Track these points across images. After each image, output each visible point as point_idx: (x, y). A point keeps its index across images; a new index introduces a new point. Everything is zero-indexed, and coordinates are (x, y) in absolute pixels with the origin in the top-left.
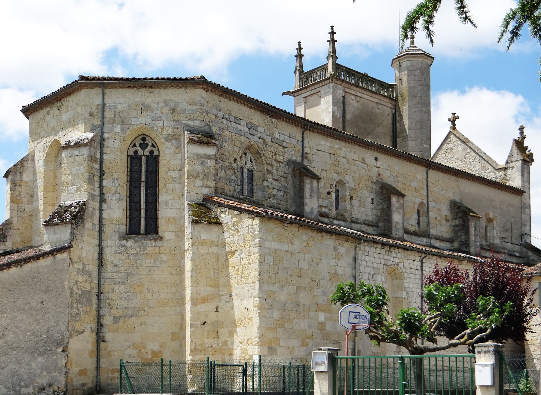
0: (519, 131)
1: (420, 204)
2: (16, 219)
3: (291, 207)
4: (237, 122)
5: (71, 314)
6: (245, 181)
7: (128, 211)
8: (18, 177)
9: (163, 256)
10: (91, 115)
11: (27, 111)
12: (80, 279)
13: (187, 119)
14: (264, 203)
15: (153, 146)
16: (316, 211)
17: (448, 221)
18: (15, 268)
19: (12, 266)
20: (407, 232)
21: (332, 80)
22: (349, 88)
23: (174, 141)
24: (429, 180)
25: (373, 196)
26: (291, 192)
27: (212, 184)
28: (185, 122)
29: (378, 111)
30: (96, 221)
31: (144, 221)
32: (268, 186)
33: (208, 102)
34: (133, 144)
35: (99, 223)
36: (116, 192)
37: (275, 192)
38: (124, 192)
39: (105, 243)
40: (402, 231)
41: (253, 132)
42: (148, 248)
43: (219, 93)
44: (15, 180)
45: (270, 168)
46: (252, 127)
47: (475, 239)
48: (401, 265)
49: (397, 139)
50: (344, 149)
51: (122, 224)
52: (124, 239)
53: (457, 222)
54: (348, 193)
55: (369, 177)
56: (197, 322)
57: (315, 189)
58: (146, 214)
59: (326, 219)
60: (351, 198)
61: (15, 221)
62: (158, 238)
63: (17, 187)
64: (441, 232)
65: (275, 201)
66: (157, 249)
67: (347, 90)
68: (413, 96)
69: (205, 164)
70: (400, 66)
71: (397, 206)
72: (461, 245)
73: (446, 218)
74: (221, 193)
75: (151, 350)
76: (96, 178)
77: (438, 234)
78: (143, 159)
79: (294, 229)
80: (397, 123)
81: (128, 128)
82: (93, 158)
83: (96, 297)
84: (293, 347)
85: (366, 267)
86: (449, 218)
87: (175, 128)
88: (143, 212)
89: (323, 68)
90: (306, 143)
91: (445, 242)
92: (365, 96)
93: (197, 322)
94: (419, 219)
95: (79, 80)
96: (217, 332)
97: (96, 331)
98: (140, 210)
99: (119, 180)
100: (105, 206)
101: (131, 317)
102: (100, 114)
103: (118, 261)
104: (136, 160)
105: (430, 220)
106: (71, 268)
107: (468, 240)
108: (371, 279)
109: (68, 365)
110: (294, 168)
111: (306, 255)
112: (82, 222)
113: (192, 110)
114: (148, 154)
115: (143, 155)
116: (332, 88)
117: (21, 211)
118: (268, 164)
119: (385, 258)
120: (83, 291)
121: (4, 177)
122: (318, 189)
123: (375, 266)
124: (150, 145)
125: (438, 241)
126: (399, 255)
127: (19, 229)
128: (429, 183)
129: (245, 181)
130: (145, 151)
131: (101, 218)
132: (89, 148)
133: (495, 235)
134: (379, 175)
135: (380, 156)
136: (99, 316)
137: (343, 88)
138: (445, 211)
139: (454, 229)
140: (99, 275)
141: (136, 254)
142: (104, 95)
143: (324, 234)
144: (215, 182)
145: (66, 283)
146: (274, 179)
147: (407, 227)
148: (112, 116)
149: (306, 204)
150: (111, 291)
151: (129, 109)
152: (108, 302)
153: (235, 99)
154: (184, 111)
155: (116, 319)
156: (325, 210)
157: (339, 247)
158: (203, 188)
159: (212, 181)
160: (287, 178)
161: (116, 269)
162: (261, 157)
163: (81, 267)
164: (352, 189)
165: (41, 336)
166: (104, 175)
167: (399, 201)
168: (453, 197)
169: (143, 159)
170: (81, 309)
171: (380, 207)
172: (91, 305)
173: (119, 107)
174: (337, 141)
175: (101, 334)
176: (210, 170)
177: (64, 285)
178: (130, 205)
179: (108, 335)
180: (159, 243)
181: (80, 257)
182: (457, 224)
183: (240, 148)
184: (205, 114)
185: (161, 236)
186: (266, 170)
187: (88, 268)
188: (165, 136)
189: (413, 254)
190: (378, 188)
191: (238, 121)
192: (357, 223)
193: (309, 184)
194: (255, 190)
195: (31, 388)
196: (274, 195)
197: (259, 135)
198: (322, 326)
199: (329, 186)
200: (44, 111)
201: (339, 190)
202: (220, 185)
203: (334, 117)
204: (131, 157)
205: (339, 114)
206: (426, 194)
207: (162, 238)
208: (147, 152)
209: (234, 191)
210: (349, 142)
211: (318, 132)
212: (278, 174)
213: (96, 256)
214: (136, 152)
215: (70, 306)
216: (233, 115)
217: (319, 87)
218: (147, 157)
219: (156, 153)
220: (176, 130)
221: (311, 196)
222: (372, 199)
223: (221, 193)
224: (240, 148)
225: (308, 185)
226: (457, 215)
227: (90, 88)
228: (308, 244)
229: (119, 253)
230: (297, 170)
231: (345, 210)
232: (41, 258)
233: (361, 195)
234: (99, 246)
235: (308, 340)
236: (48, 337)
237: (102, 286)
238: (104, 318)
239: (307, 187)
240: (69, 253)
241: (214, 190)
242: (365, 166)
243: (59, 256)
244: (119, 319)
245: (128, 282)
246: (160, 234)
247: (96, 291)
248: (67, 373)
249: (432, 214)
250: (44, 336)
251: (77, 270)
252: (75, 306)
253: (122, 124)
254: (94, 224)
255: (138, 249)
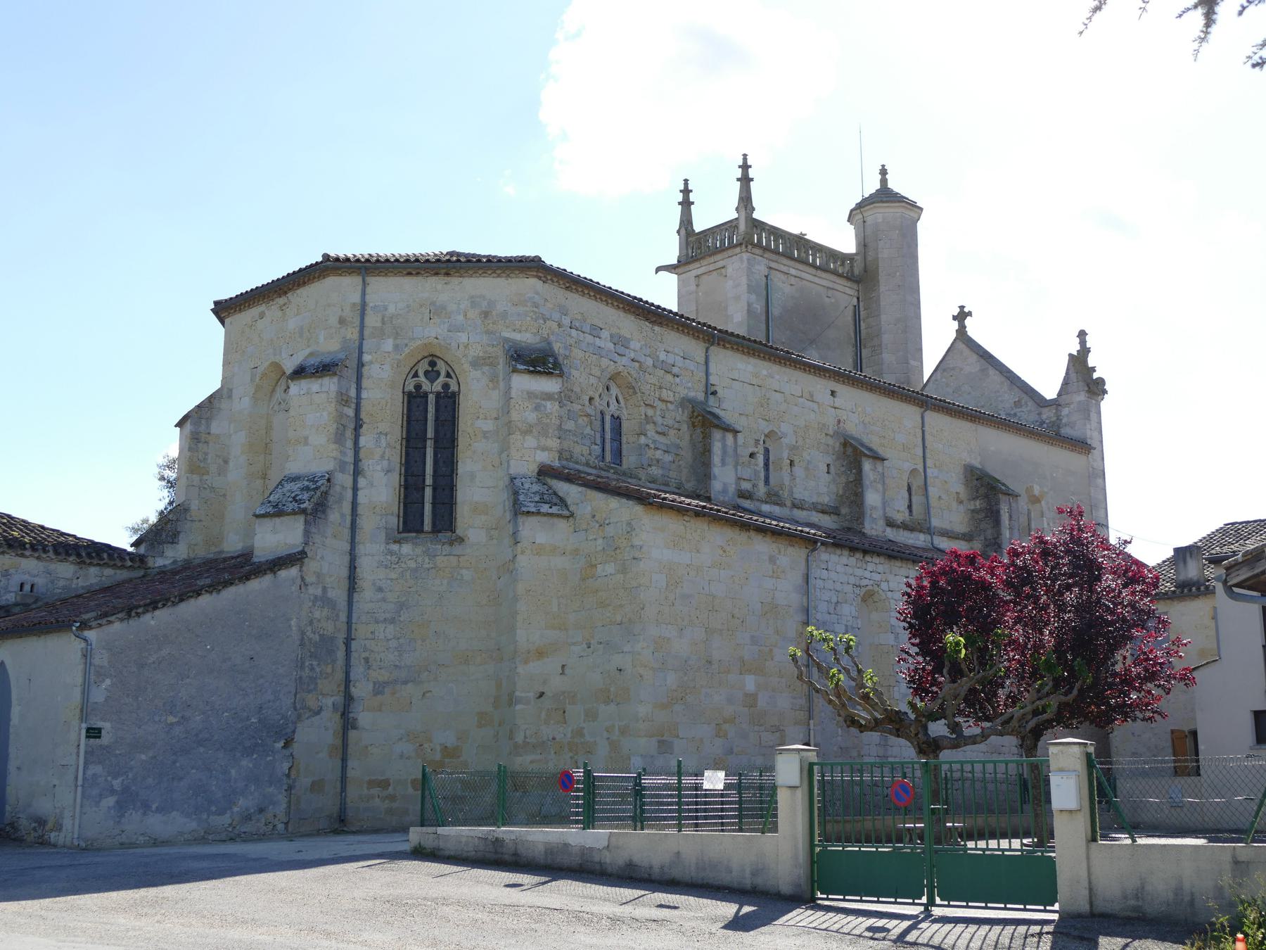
0: (1078, 340)
1: (911, 471)
2: (197, 502)
3: (688, 481)
4: (595, 333)
5: (301, 678)
6: (608, 436)
7: (402, 490)
8: (202, 428)
9: (464, 572)
10: (342, 321)
11: (223, 310)
12: (317, 614)
13: (509, 330)
14: (640, 476)
15: (448, 375)
16: (732, 489)
17: (961, 502)
18: (208, 595)
19: (203, 592)
20: (890, 523)
21: (746, 247)
22: (776, 262)
23: (487, 368)
24: (927, 428)
25: (829, 460)
26: (687, 454)
27: (554, 443)
28: (506, 334)
29: (827, 299)
30: (347, 507)
31: (431, 509)
32: (647, 445)
33: (546, 300)
34: (413, 372)
35: (352, 511)
36: (382, 457)
37: (658, 454)
38: (395, 456)
39: (361, 549)
40: (881, 523)
41: (621, 350)
42: (437, 558)
43: (564, 284)
44: (198, 433)
45: (650, 412)
46: (620, 342)
47: (1011, 534)
48: (884, 586)
49: (863, 350)
50: (777, 377)
51: (392, 514)
52: (395, 542)
53: (978, 504)
54: (785, 455)
55: (820, 425)
56: (528, 694)
57: (730, 451)
58: (434, 497)
59: (749, 501)
60: (792, 463)
61: (194, 505)
62: (456, 540)
63: (200, 445)
64: (951, 522)
65: (660, 472)
66: (453, 559)
67: (773, 265)
68: (889, 275)
69: (543, 408)
70: (864, 222)
71: (872, 478)
72: (987, 546)
73: (958, 497)
74: (567, 459)
75: (441, 744)
76: (349, 434)
77: (944, 526)
78: (431, 398)
79: (700, 526)
80: (862, 322)
81: (406, 345)
82: (345, 399)
83: (343, 648)
84: (701, 740)
85: (823, 591)
86: (963, 496)
87: (488, 345)
88: (428, 492)
89: (730, 227)
90: (712, 369)
91: (957, 541)
92: (804, 275)
93: (528, 694)
94: (910, 500)
95: (322, 262)
96: (564, 712)
97: (341, 709)
98: (424, 489)
99: (389, 437)
100: (362, 482)
101: (405, 683)
102: (357, 321)
103: (384, 581)
104: (419, 399)
105: (930, 502)
106: (302, 595)
107: (998, 537)
108: (832, 612)
109: (293, 772)
110: (693, 412)
111: (722, 571)
112: (324, 512)
113: (519, 315)
114: (439, 389)
115: (431, 392)
116: (746, 261)
117: (204, 488)
118: (646, 405)
119: (856, 574)
120: (321, 636)
121: (176, 426)
122: (735, 450)
123: (838, 586)
124: (443, 373)
125: (945, 539)
126: (880, 568)
127: (200, 521)
128: (926, 433)
129: (608, 436)
130: (435, 384)
131: (354, 505)
132: (339, 380)
133: (1046, 526)
134: (839, 421)
135: (839, 388)
136: (347, 681)
137: (765, 261)
138: (957, 485)
139: (973, 517)
140: (349, 605)
141: (416, 570)
142: (365, 288)
143: (752, 533)
144: (559, 441)
145: (293, 623)
146: (658, 433)
147: (890, 515)
148: (379, 324)
149: (715, 477)
150: (371, 636)
151: (408, 312)
152: (364, 655)
153: (592, 294)
154: (504, 315)
155: (379, 689)
156: (746, 486)
157: (777, 556)
158: (538, 452)
159: (555, 439)
160: (679, 430)
161: (380, 596)
162: (635, 393)
163: (319, 592)
164: (793, 448)
165: (248, 718)
166: (361, 426)
167: (876, 468)
168: (968, 460)
169: (431, 398)
170: (318, 670)
171: (843, 479)
172: (334, 661)
173: (391, 309)
174: (766, 364)
175: (351, 715)
176: (551, 419)
177: (290, 626)
178: (406, 481)
179: (364, 717)
180: (457, 549)
181: (318, 575)
182: (978, 507)
183: (599, 378)
184: (542, 322)
185: (461, 535)
186: (643, 417)
187: (331, 594)
188: (470, 359)
189: (904, 566)
190: (838, 444)
191: (596, 331)
192: (802, 509)
193: (719, 441)
194: (624, 453)
195: (228, 815)
196: (658, 461)
197: (632, 355)
198: (751, 700)
199: (752, 442)
200: (254, 311)
201: (770, 448)
202: (566, 445)
203: (750, 311)
204: (410, 395)
205: (759, 307)
206: (921, 454)
207: (463, 540)
208: (437, 386)
209: (590, 454)
210: (785, 364)
211: (732, 348)
212: (665, 423)
213: (345, 572)
214: (418, 387)
215: (299, 664)
216: (588, 321)
217: (723, 259)
218: (438, 395)
219: (454, 387)
220: (490, 349)
221: (723, 463)
222: (828, 465)
223: (567, 459)
224: (599, 378)
225: (718, 443)
226: (977, 492)
227: (341, 275)
228: (724, 551)
229: (386, 567)
230: (699, 415)
231: (782, 486)
232: (253, 577)
233: (808, 458)
234: (351, 554)
235: (726, 726)
236: (260, 721)
237: (354, 626)
238: (357, 684)
239: (717, 448)
240: (301, 567)
241: (557, 456)
242: (815, 406)
243: (283, 574)
244: (384, 687)
245: (402, 619)
246: (459, 532)
247: (341, 636)
248: (290, 788)
249: (933, 491)
250: (253, 720)
251: (312, 598)
252: (307, 664)
253: (396, 338)
254: (343, 516)
255: (420, 560)
